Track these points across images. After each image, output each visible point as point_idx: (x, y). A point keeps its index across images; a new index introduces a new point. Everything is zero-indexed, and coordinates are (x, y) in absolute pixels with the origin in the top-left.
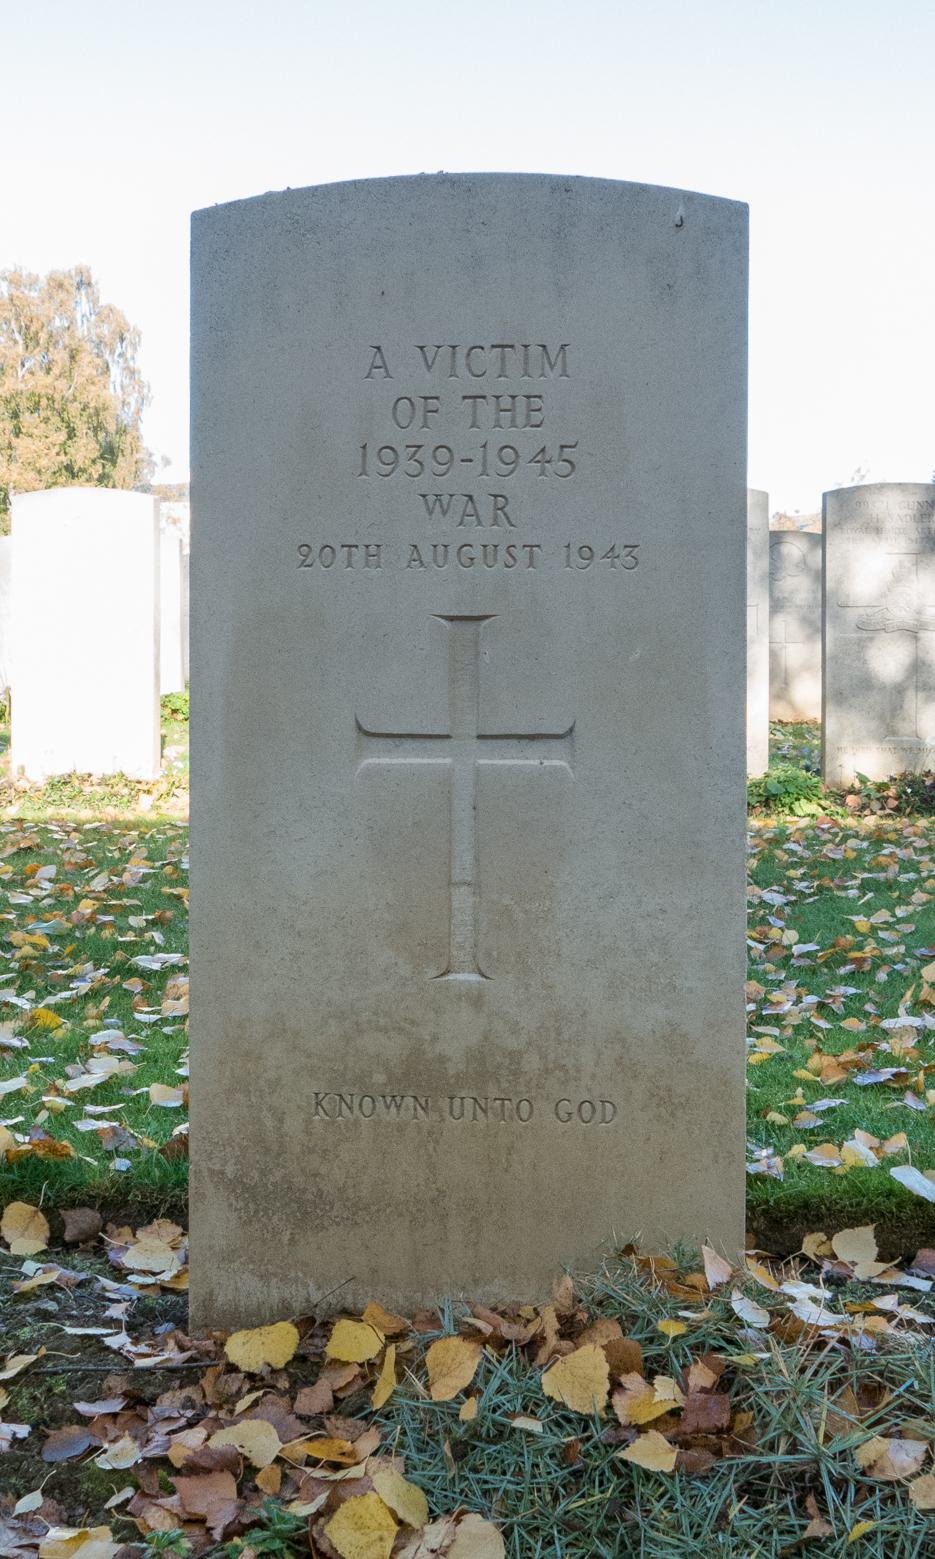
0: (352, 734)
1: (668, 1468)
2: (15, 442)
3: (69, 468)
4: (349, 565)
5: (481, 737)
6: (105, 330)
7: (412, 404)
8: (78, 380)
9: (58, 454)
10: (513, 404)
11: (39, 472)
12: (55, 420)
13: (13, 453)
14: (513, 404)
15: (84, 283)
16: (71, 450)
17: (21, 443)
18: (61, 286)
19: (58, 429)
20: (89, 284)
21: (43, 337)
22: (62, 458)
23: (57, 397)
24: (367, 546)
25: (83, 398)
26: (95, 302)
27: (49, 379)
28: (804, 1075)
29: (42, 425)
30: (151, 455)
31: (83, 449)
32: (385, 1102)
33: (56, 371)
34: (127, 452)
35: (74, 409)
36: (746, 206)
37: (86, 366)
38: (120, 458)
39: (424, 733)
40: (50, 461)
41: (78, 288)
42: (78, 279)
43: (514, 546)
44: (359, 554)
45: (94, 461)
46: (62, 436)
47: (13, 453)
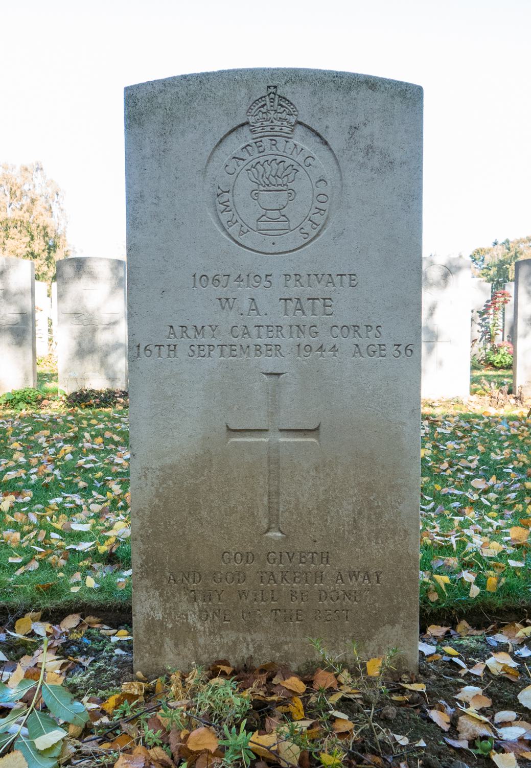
0: (225, 429)
1: (489, 705)
2: (6, 242)
3: (32, 254)
4: (160, 356)
5: (281, 430)
6: (50, 190)
7: (349, 330)
8: (35, 213)
9: (26, 247)
10: (175, 348)
11: (17, 255)
12: (24, 231)
13: (5, 247)
14: (175, 348)
15: (39, 169)
16: (32, 246)
17: (9, 242)
18: (26, 169)
19: (26, 236)
20: (42, 169)
21: (18, 193)
22: (28, 249)
23: (25, 221)
24: (169, 346)
25: (38, 222)
26: (45, 177)
27: (21, 213)
28: (427, 411)
29: (19, 234)
30: (74, 248)
31: (38, 245)
32: (289, 556)
33: (25, 208)
34: (61, 247)
35: (34, 226)
36: (420, 89)
37: (39, 208)
38: (58, 249)
39: (286, 428)
40: (23, 250)
41: (37, 171)
42: (37, 167)
43: (380, 326)
44: (164, 350)
45: (43, 251)
46: (28, 239)
47: (5, 247)
